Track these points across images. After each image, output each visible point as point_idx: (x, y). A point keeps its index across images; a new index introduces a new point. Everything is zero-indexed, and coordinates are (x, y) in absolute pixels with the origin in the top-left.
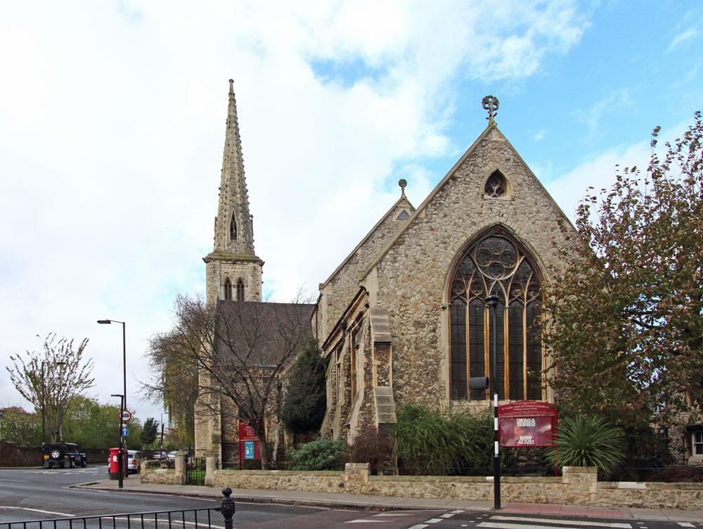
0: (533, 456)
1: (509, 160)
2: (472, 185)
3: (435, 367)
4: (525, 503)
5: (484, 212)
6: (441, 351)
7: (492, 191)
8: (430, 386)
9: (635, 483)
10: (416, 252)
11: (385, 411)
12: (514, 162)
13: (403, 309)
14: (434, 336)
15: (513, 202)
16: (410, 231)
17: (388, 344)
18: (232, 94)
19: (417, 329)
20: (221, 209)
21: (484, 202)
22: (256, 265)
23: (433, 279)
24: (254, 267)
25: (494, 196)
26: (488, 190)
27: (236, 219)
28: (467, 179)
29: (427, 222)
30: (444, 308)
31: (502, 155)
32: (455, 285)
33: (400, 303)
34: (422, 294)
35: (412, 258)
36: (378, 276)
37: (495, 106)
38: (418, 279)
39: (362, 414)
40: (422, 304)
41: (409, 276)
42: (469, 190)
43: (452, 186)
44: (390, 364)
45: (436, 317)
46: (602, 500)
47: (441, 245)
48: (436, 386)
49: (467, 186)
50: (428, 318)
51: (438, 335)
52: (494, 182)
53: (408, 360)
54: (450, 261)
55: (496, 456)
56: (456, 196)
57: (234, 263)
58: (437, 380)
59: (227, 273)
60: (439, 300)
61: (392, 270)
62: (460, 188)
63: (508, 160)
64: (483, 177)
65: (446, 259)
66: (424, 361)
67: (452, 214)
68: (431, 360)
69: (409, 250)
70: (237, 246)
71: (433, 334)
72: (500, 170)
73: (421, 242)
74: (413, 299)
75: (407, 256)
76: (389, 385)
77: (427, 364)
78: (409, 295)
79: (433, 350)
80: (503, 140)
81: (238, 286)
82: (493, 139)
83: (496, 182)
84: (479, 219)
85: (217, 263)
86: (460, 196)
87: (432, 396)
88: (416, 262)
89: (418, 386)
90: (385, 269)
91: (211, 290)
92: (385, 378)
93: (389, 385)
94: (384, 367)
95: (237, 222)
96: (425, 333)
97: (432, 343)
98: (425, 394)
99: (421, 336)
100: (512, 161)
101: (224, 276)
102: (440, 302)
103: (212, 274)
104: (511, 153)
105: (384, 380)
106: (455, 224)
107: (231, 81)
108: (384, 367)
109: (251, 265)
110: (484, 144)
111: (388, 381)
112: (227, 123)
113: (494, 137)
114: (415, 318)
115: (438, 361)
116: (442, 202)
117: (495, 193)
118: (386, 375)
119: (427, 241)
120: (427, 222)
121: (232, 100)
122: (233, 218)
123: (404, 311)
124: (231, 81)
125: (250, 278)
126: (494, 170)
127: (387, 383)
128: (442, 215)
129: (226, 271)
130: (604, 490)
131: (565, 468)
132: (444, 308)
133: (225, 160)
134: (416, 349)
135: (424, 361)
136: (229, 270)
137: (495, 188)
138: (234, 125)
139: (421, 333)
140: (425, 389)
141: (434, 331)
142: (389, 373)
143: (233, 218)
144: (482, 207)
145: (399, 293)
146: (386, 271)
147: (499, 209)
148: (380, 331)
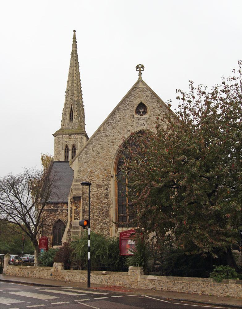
0: (164, 262)
1: (148, 96)
2: (128, 111)
3: (107, 209)
4: (164, 292)
5: (134, 124)
6: (110, 200)
7: (140, 113)
8: (104, 220)
9: (153, 276)
10: (98, 148)
11: (76, 234)
12: (151, 97)
13: (91, 178)
14: (107, 192)
15: (151, 118)
16: (96, 138)
17: (80, 197)
18: (75, 38)
19: (98, 189)
20: (66, 104)
21: (134, 119)
22: (82, 136)
23: (107, 162)
24: (82, 137)
25: (141, 115)
26: (138, 112)
27: (73, 109)
28: (125, 109)
29: (104, 133)
30: (112, 177)
31: (144, 94)
32: (119, 163)
33: (90, 175)
34: (101, 170)
35: (96, 152)
36: (79, 162)
37: (142, 69)
38: (99, 162)
39: (68, 235)
40: (101, 175)
41: (94, 161)
42: (126, 114)
43: (117, 113)
44: (81, 208)
45: (108, 182)
46: (142, 285)
47: (111, 144)
48: (108, 219)
49: (125, 112)
50: (103, 182)
51: (109, 192)
52: (141, 108)
53: (92, 206)
54: (116, 151)
55: (88, 260)
56: (119, 117)
57: (70, 136)
58: (108, 216)
59: (66, 142)
60: (110, 173)
61: (85, 159)
62: (122, 113)
63: (147, 96)
64: (134, 107)
65: (114, 150)
66: (101, 206)
67: (117, 127)
68: (105, 205)
69: (95, 147)
70: (73, 125)
71: (106, 191)
72: (143, 102)
73: (101, 143)
74: (96, 173)
75: (93, 150)
76: (80, 220)
77: (103, 208)
78: (94, 171)
79: (106, 200)
80: (145, 86)
81: (73, 149)
82: (140, 87)
83: (141, 108)
84: (132, 128)
85: (61, 136)
86: (121, 117)
87: (106, 225)
88: (98, 153)
89: (98, 220)
90: (82, 158)
91: (57, 152)
92: (78, 216)
93: (80, 220)
94: (78, 210)
95: (73, 111)
96: (102, 191)
97: (106, 196)
98: (101, 224)
99: (100, 192)
100: (150, 96)
101: (64, 144)
102: (110, 174)
103: (57, 143)
104: (149, 92)
105: (77, 217)
106: (119, 132)
107: (75, 31)
108: (78, 210)
109: (80, 136)
110: (134, 90)
111: (79, 217)
112: (71, 55)
113: (141, 85)
114: (97, 183)
115: (109, 206)
116: (112, 121)
117: (141, 114)
118: (78, 214)
119: (104, 142)
120: (104, 133)
121: (75, 42)
122: (72, 109)
123: (91, 179)
124: (75, 31)
125: (79, 144)
126: (140, 102)
127: (79, 219)
128: (112, 128)
129: (66, 140)
130: (143, 280)
131: (130, 268)
132: (112, 177)
133: (69, 75)
134: (97, 199)
135: (101, 206)
136: (67, 140)
137: (141, 111)
138: (75, 55)
139: (100, 190)
140: (102, 222)
141: (107, 189)
142: (80, 213)
143: (72, 109)
144: (133, 122)
145: (89, 170)
146: (82, 159)
147: (142, 122)
148: (76, 191)
